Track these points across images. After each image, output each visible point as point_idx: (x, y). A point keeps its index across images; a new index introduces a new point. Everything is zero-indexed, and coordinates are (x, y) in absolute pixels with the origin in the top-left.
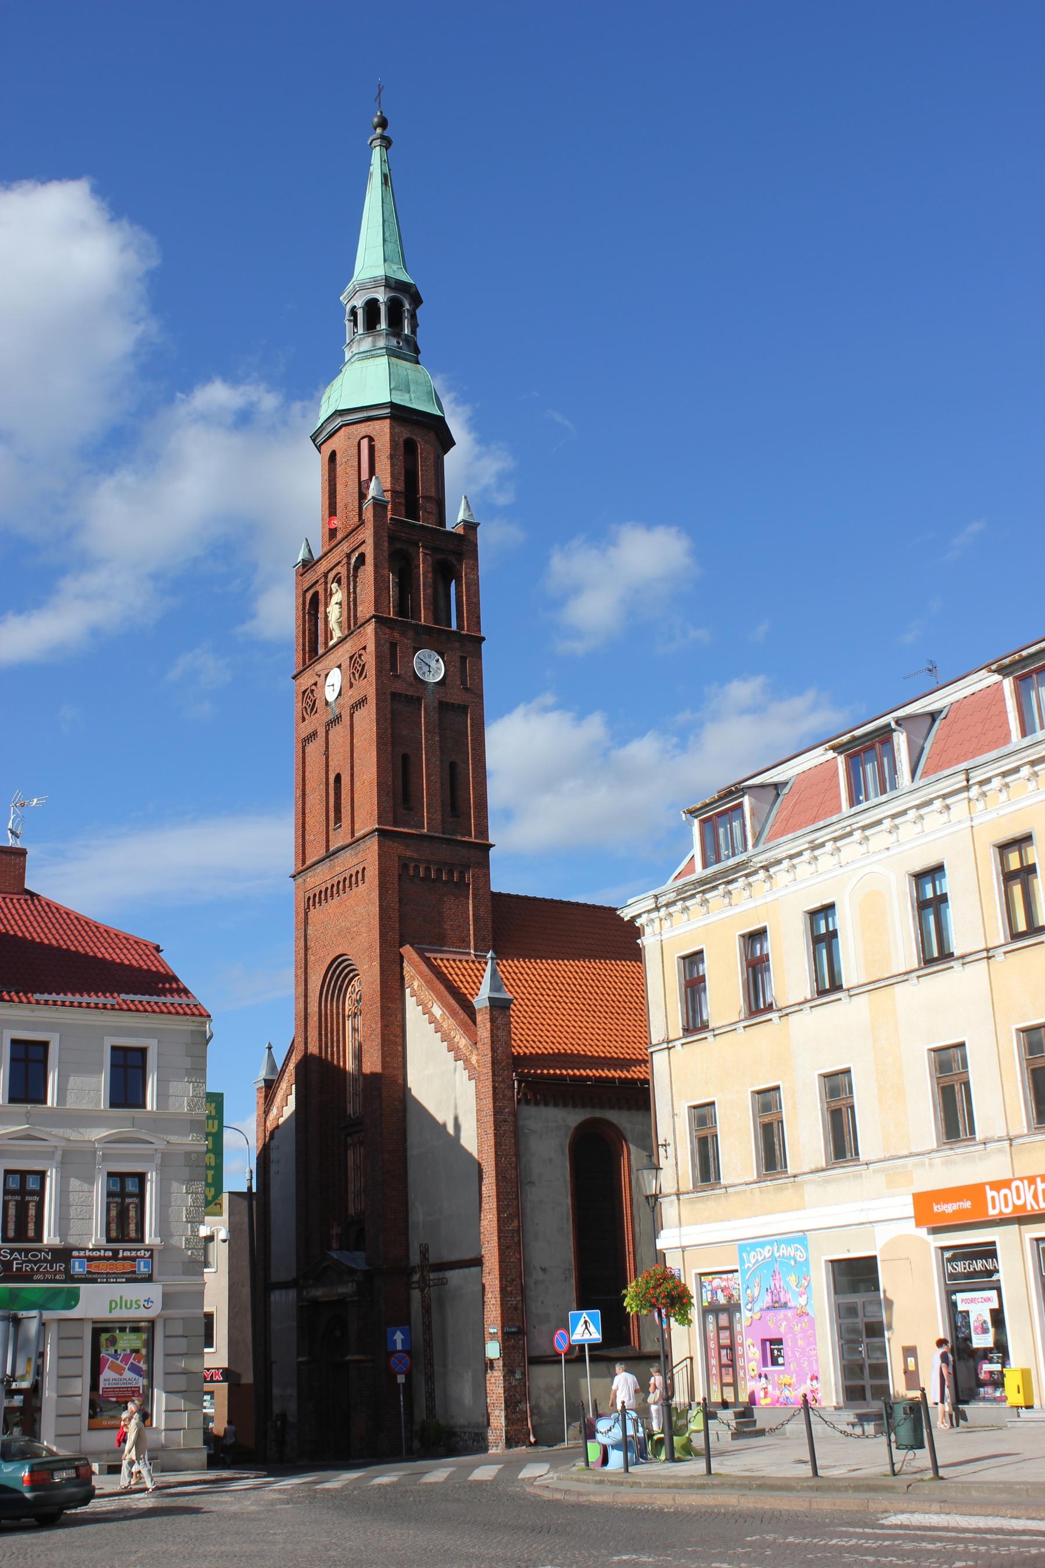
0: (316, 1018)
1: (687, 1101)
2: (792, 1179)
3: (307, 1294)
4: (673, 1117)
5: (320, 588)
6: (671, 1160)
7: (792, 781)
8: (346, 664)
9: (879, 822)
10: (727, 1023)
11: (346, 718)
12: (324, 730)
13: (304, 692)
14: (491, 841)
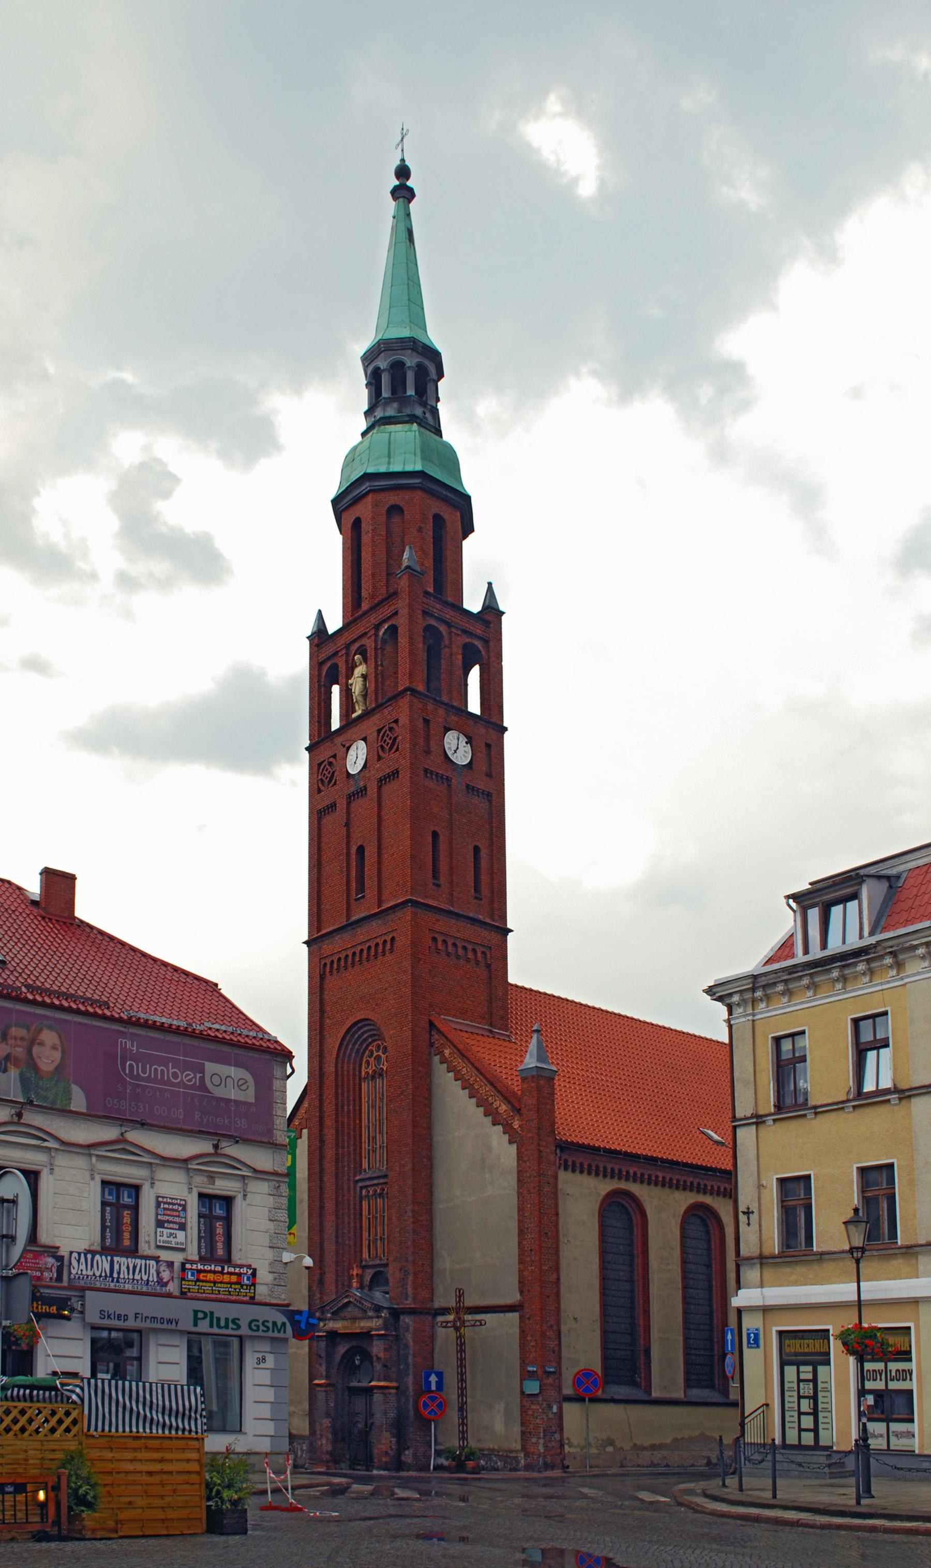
0: (332, 1078)
1: (776, 1174)
3: (325, 1325)
4: (759, 1188)
7: (904, 875)
8: (373, 736)
10: (830, 1101)
11: (372, 791)
12: (345, 802)
13: (320, 765)
14: (509, 926)
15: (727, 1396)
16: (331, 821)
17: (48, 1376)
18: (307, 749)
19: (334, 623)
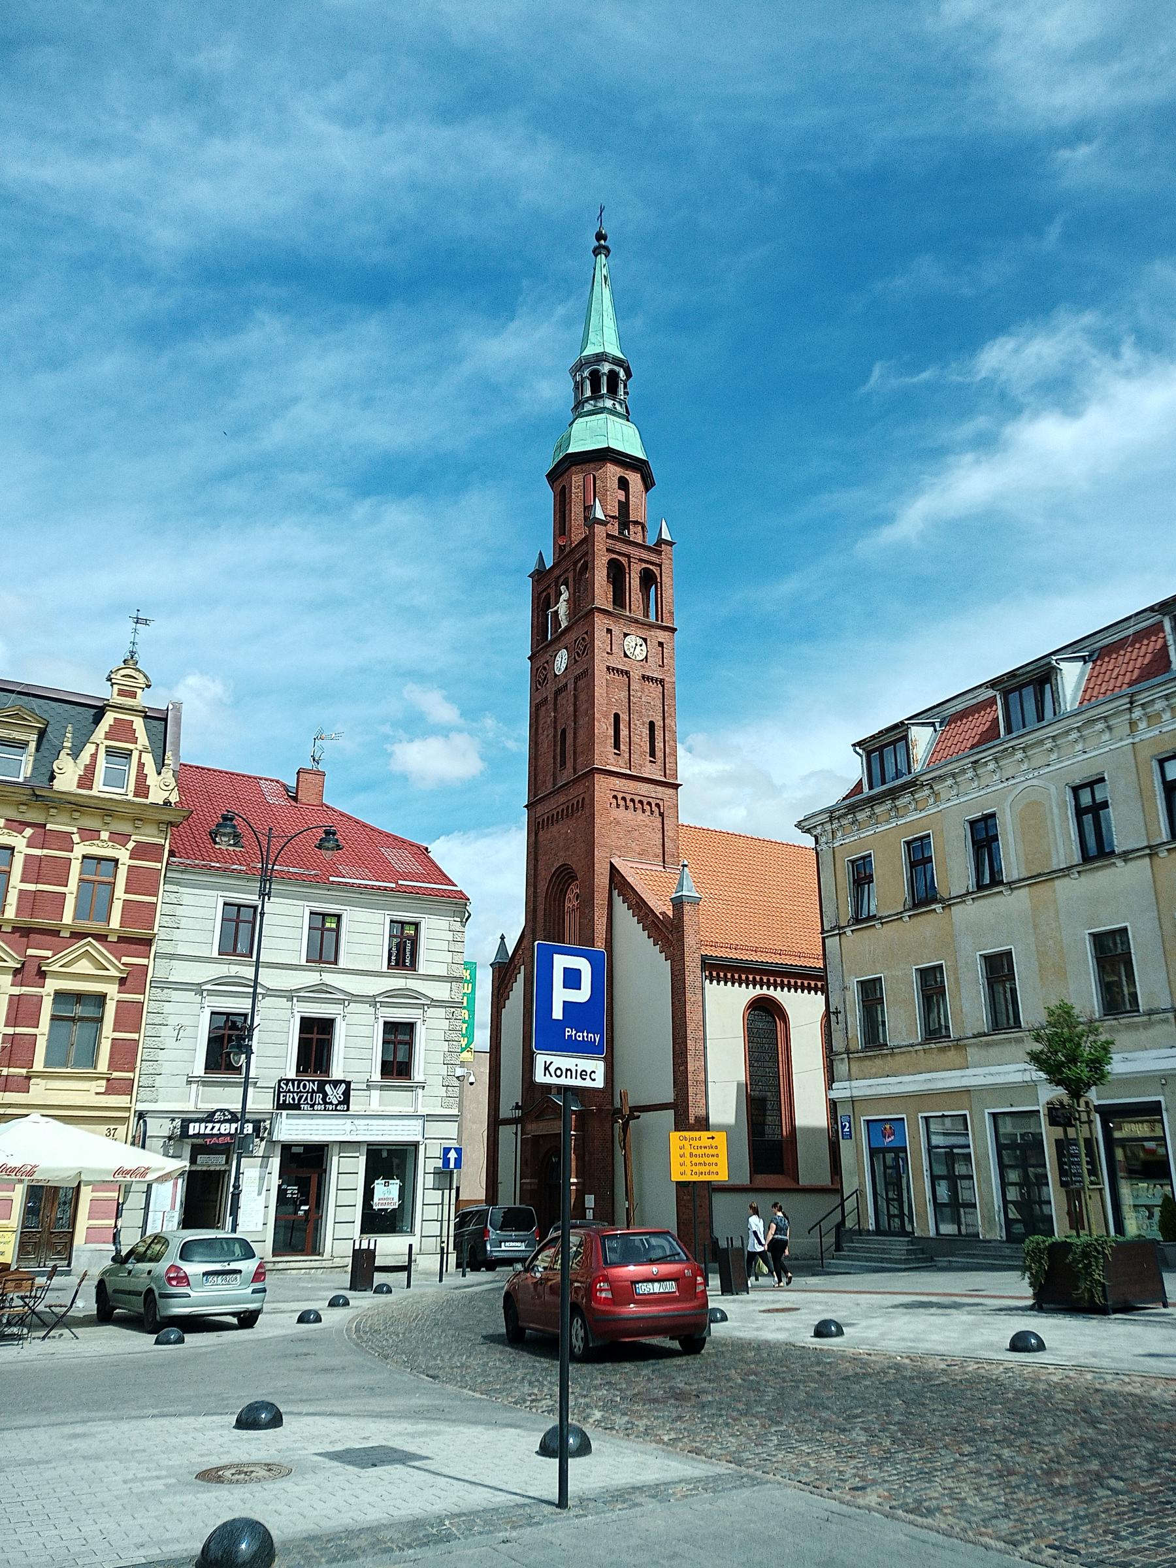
2: (1145, 1018)
5: (552, 592)
6: (842, 1025)
9: (1041, 742)
11: (571, 687)
15: (796, 1179)
16: (548, 715)
17: (1026, 1278)
18: (529, 658)
19: (549, 564)
